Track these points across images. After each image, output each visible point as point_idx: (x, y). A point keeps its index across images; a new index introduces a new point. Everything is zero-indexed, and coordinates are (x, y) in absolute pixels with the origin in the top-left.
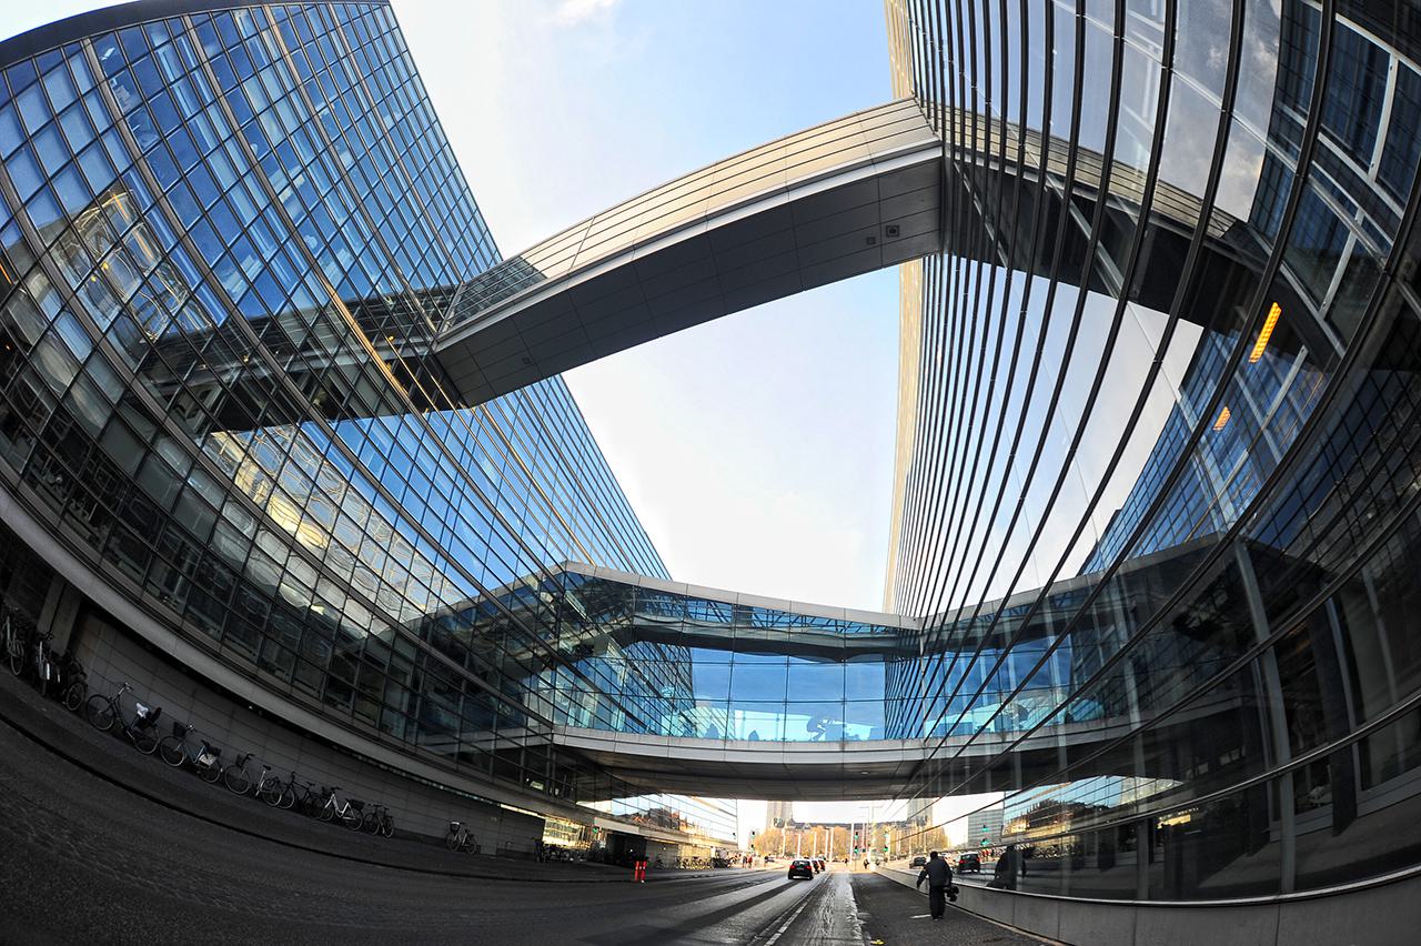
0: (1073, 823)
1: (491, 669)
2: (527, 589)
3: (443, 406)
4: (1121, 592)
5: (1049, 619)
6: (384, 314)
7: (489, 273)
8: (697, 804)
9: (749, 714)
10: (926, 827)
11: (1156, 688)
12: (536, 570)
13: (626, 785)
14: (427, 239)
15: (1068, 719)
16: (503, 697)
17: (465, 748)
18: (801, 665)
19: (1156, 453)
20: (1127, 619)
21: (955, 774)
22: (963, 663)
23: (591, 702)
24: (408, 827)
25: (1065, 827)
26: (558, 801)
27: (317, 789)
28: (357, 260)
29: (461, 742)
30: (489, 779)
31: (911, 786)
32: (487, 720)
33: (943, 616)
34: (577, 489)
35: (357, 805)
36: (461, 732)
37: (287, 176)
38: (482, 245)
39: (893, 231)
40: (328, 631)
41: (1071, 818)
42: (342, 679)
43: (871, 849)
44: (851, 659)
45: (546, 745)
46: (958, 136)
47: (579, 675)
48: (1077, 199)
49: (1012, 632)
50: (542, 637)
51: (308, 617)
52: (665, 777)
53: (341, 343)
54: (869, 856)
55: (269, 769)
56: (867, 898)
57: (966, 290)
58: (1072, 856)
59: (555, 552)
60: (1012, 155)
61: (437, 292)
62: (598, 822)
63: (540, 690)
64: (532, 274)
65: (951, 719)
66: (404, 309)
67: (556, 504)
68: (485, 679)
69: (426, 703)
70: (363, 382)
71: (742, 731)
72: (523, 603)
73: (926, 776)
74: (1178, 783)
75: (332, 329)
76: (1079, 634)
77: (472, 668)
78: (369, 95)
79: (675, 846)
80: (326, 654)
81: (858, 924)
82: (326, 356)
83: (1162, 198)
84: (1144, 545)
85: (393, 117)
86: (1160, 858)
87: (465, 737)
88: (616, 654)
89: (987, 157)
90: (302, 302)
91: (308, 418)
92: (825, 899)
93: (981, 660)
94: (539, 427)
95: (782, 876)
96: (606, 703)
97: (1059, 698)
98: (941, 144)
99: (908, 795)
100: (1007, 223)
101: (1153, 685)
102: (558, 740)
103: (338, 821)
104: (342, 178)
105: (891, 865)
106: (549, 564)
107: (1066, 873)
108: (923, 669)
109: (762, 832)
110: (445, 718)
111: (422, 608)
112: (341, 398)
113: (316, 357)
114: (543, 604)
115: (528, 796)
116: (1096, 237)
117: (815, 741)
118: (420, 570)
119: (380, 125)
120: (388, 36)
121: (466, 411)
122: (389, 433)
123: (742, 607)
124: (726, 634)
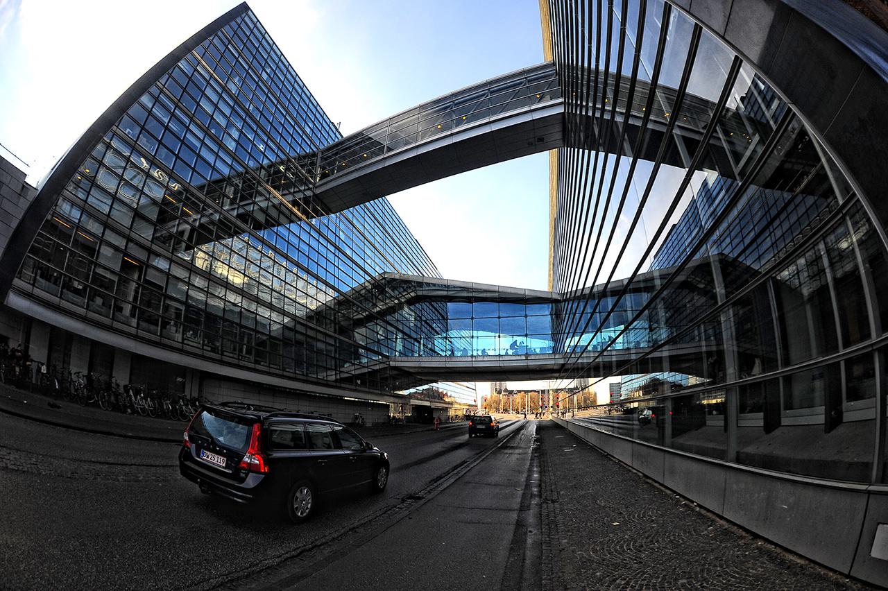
3: (319, 214)
14: (299, 134)
33: (580, 291)
38: (288, 75)
45: (386, 368)
59: (376, 268)
61: (307, 156)
102: (392, 364)
109: (489, 397)
121: (333, 215)
122: (297, 233)
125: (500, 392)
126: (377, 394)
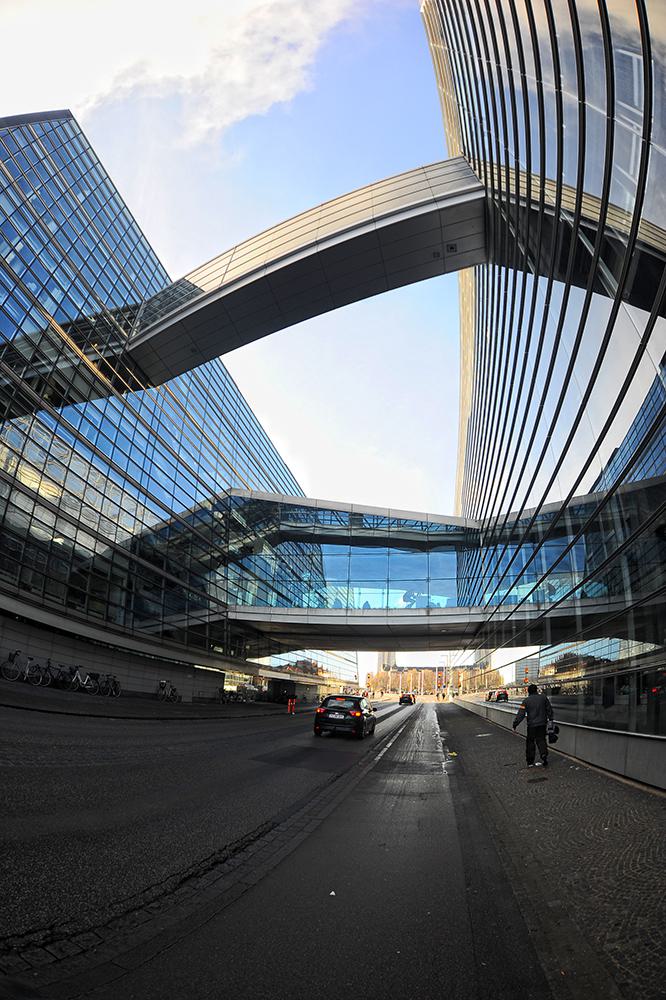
0: (587, 671)
1: (182, 569)
2: (204, 510)
3: (136, 388)
4: (619, 506)
5: (569, 523)
6: (89, 329)
7: (163, 292)
8: (329, 655)
9: (363, 590)
10: (488, 669)
11: (644, 577)
12: (210, 496)
13: (279, 644)
14: (116, 273)
15: (583, 595)
16: (192, 588)
17: (167, 627)
18: (398, 554)
19: (643, 409)
20: (623, 526)
21: (506, 632)
22: (510, 553)
23: (253, 587)
24: (131, 688)
25: (581, 674)
26: (233, 660)
27: (66, 669)
28: (66, 294)
29: (164, 623)
30: (185, 648)
31: (476, 641)
32: (181, 606)
34: (236, 437)
35: (94, 677)
36: (163, 616)
37: (10, 245)
38: (157, 274)
39: (452, 248)
40: (70, 555)
41: (585, 667)
42: (78, 588)
43: (449, 685)
44: (435, 549)
46: (496, 183)
47: (244, 568)
48: (582, 227)
49: (544, 532)
50: (217, 543)
51: (52, 547)
52: (305, 637)
53: (60, 353)
54: (448, 691)
55: (31, 659)
56: (447, 721)
57: (506, 289)
58: (585, 694)
59: (222, 484)
60: (536, 196)
61: (126, 309)
62: (262, 672)
63: (216, 581)
64: (194, 290)
65: (503, 593)
66: (104, 324)
67: (222, 449)
68: (178, 577)
69: (139, 598)
70: (78, 378)
71: (359, 603)
72: (201, 521)
73: (486, 633)
74: (658, 647)
75: (53, 344)
76: (590, 535)
77: (169, 569)
78: (64, 182)
79: (315, 687)
80: (66, 571)
81: (441, 740)
82: (50, 363)
83: (644, 232)
84: (635, 474)
85: (84, 194)
86: (645, 701)
87: (166, 619)
88: (269, 552)
89: (517, 197)
90: (29, 329)
91: (41, 408)
92: (418, 722)
93: (523, 551)
94: (206, 395)
95: (394, 704)
96: (263, 587)
97: (577, 580)
98: (484, 188)
99: (474, 647)
100: (534, 244)
101: (641, 575)
102: (232, 616)
103: (82, 690)
104: (50, 240)
105: (462, 697)
106: (219, 492)
107: (581, 707)
108: (483, 556)
109: (375, 674)
110: (152, 608)
111: (131, 530)
112: (63, 391)
113: (43, 366)
114: (216, 520)
115: (213, 657)
116: (597, 254)
117: (408, 608)
118: (128, 504)
119: (75, 201)
120: (75, 141)
121: (153, 389)
123: (355, 514)
124: (345, 533)
125: (388, 669)
126: (201, 656)
